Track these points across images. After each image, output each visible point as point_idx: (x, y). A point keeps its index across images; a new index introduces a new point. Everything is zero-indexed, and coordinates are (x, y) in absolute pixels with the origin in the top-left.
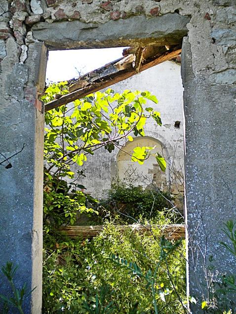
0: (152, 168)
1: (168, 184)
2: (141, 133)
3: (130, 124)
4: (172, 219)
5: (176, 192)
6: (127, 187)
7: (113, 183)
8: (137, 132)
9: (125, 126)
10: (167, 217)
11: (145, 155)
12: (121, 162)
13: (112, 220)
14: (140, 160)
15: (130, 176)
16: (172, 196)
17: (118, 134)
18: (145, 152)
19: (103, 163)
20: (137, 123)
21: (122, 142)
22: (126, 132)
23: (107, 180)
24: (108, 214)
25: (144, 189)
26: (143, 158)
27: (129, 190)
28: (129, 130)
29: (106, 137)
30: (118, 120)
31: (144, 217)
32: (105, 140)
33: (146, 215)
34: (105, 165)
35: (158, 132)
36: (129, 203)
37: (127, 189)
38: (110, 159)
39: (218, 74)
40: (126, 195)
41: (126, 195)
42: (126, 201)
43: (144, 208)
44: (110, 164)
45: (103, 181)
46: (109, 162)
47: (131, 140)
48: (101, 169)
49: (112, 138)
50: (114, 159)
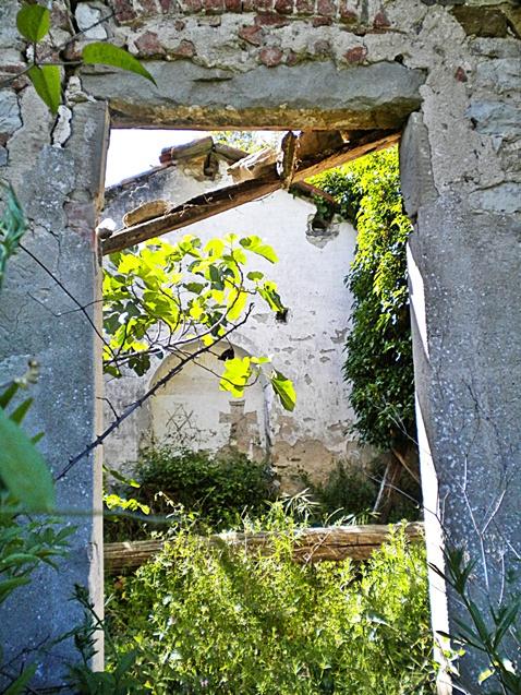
1: (263, 444)
5: (282, 461)
6: (177, 454)
11: (248, 375)
14: (237, 387)
16: (275, 470)
19: (119, 400)
23: (128, 439)
26: (241, 382)
42: (177, 486)
43: (219, 499)
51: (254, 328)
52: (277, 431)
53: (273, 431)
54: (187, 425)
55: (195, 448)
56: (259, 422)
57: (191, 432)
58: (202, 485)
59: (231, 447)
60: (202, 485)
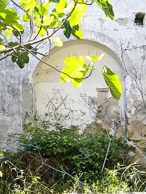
0: (94, 94)
1: (123, 123)
2: (77, 33)
3: (57, 16)
4: (131, 184)
5: (137, 137)
6: (52, 129)
7: (27, 122)
8: (69, 30)
9: (48, 20)
10: (124, 180)
11: (84, 70)
12: (41, 86)
13: (27, 186)
14: (77, 80)
15: (56, 109)
16: (130, 143)
17: (34, 35)
18: (84, 65)
19: (9, 86)
20: (69, 15)
21: (43, 49)
22: (51, 31)
23: (16, 116)
24: (20, 174)
25: (80, 132)
26: (80, 76)
27: (56, 134)
28: (55, 26)
29: (15, 39)
30: (36, 9)
31: (82, 180)
32: (11, 44)
33: (86, 178)
34: (13, 91)
35: (106, 32)
36: (54, 156)
37: (50, 133)
38: (21, 79)
39: (104, 92)
40: (50, 143)
41: (50, 143)
42: (49, 153)
43: (81, 165)
44: (21, 88)
45: (9, 119)
46: (19, 84)
47: (60, 44)
48: (4, 98)
49: (25, 41)
50: (28, 80)
51: (117, 30)
52: (133, 112)
53: (130, 112)
54: (62, 107)
55: (67, 124)
56: (120, 105)
57: (65, 112)
58: (69, 153)
59: (97, 125)
60: (69, 153)
